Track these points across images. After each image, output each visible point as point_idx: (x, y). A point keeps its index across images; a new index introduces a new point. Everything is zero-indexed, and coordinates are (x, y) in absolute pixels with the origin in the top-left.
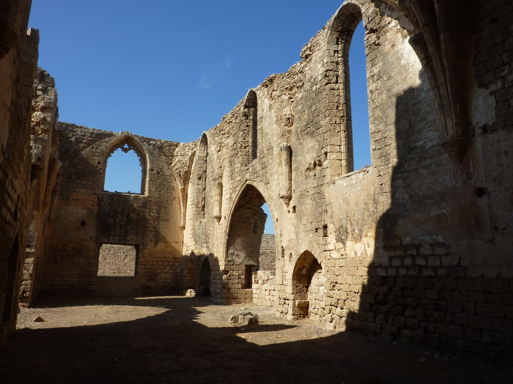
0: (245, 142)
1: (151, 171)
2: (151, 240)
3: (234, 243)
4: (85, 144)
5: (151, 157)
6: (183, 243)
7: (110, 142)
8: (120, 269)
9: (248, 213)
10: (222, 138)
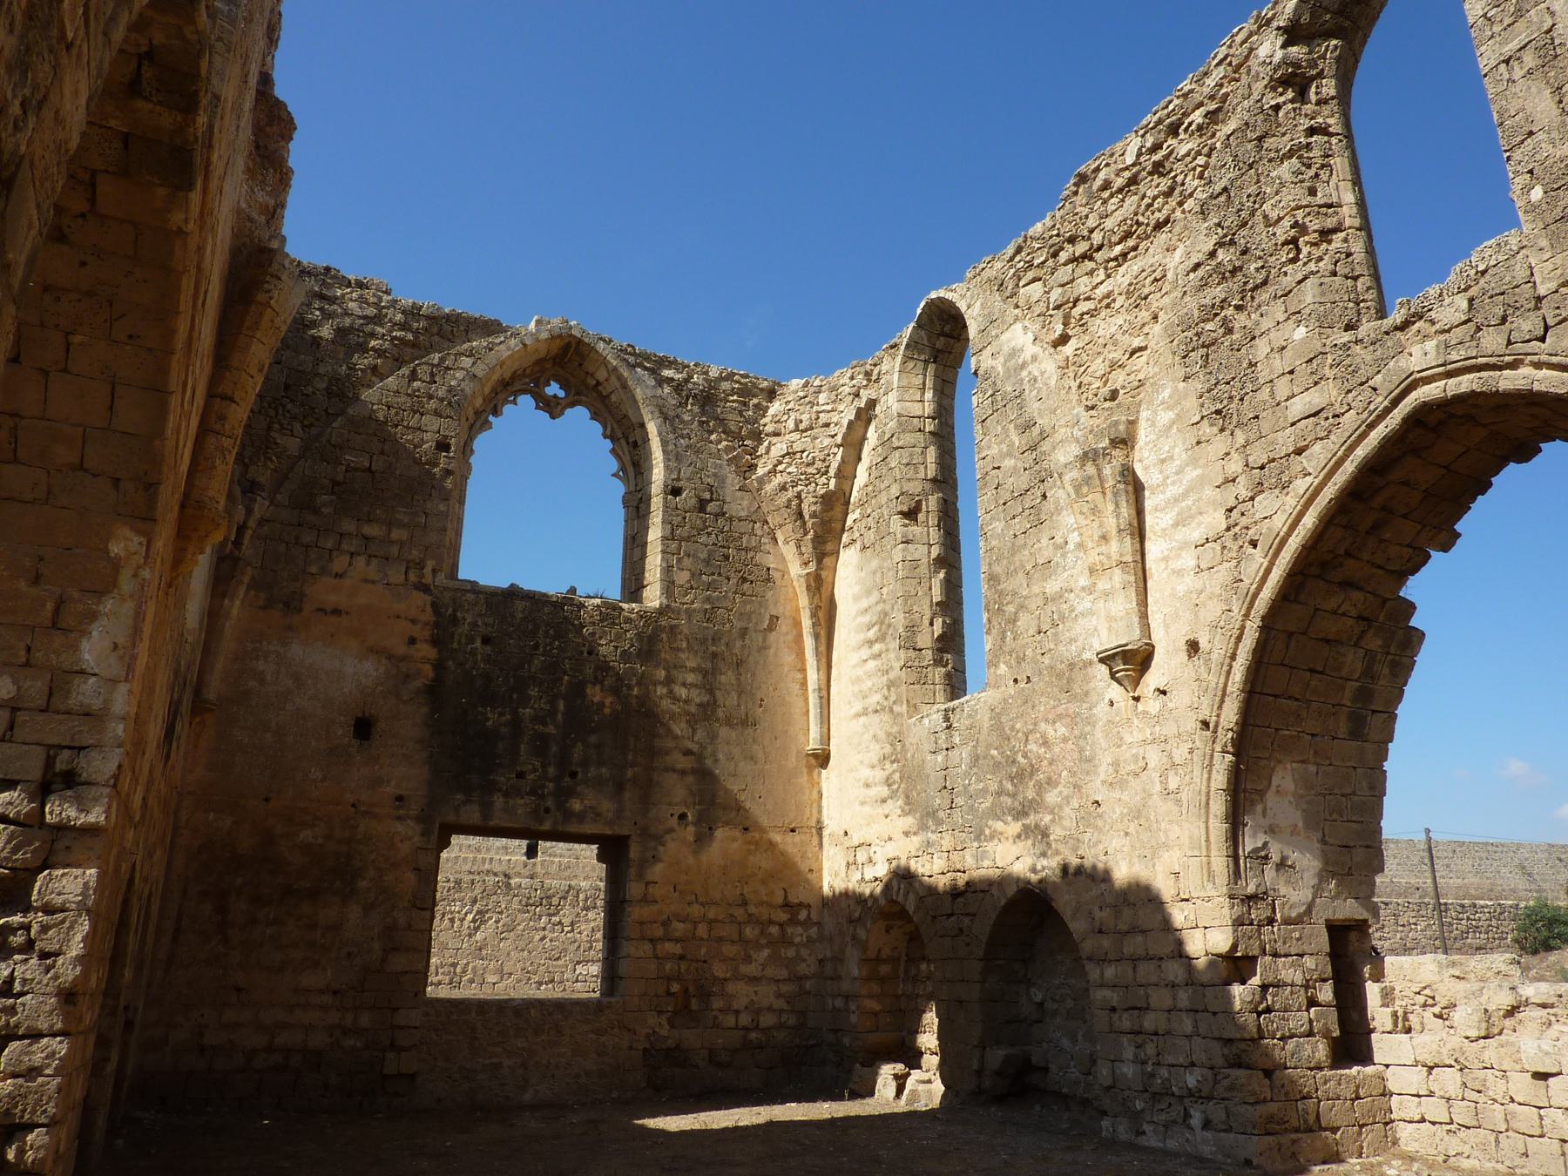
0: (1320, 206)
1: (670, 497)
2: (683, 817)
3: (1262, 793)
4: (379, 356)
5: (671, 436)
6: (820, 830)
7: (491, 358)
8: (459, 970)
9: (1344, 614)
10: (1072, 281)
